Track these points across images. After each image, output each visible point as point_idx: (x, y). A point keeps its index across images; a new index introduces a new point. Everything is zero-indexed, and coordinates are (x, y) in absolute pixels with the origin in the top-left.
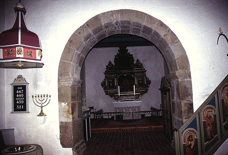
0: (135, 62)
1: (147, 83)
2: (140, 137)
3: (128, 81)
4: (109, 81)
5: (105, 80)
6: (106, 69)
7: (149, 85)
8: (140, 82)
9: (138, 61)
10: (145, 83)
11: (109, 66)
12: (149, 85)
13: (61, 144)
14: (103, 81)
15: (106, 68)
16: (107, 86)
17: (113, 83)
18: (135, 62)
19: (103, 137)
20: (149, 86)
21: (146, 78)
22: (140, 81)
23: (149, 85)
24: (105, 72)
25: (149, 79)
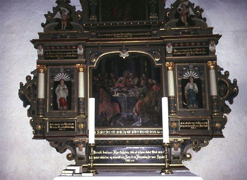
0: (29, 107)
1: (219, 91)
2: (127, 74)
3: (136, 80)
4: (52, 77)
5: (36, 73)
6: (43, 25)
7: (231, 102)
8: (190, 86)
9: (25, 106)
10: (214, 92)
11: (58, 15)
12: (227, 103)
13: (38, 135)
14: (28, 78)
15: (45, 23)
16: (45, 100)
17: (72, 86)
18: (29, 107)
19: (92, 140)
20: (231, 106)
21: (218, 69)
22: (188, 81)
23: (231, 102)
24: (37, 37)
25: (227, 74)
